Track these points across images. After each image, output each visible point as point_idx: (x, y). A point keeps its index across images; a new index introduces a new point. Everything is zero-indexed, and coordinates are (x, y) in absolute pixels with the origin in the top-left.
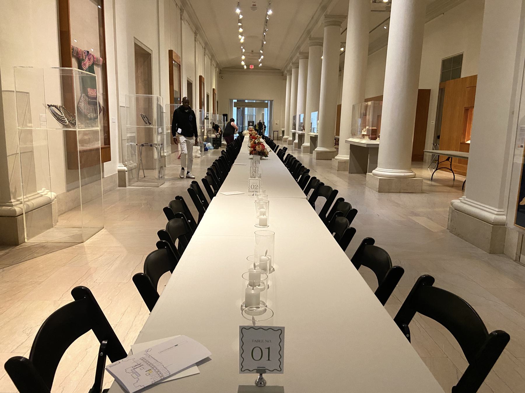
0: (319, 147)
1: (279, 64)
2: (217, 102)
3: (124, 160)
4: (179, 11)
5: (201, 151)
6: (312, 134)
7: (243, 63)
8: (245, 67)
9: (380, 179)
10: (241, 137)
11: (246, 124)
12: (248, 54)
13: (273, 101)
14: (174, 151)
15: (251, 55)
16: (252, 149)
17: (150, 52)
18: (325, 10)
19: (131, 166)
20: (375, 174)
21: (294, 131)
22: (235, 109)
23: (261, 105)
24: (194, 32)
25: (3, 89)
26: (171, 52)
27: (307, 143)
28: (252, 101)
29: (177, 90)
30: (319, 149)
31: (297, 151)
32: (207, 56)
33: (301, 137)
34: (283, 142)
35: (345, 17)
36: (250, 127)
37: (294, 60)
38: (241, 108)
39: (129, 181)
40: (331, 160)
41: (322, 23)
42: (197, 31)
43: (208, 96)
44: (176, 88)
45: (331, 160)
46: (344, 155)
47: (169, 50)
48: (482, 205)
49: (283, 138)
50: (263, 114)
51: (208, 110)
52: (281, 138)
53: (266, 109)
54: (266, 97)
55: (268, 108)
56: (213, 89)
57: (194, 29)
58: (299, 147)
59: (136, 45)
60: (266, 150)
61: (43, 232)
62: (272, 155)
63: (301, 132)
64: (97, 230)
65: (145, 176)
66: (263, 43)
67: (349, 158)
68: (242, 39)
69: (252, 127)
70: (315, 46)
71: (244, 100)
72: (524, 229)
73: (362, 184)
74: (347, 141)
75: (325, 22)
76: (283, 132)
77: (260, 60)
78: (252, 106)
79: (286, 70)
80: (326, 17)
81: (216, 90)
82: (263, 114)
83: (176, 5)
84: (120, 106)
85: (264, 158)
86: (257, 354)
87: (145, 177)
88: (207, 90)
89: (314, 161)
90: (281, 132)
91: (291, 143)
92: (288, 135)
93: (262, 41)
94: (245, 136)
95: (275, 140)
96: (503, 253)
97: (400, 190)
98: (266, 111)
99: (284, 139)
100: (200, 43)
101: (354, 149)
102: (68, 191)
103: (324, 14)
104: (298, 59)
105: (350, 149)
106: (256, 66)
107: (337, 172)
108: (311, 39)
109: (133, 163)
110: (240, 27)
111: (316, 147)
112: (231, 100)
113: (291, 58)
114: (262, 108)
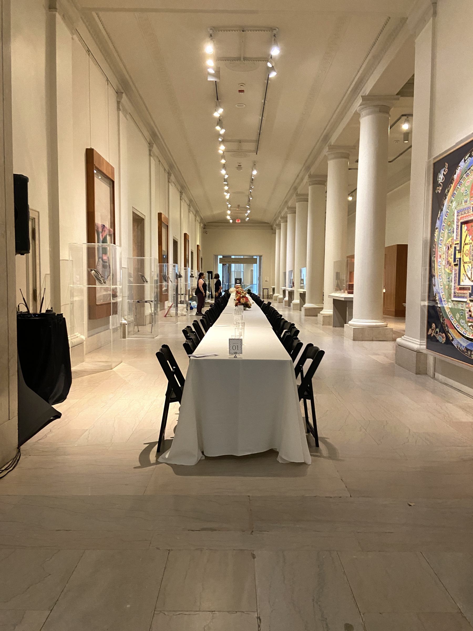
0: (355, 318)
1: (268, 218)
2: (202, 258)
3: (124, 315)
4: (167, 175)
5: (187, 310)
6: (302, 291)
7: (228, 217)
8: (231, 221)
9: (354, 328)
10: (228, 295)
11: (233, 282)
12: (235, 209)
13: (262, 256)
14: (161, 309)
15: (237, 209)
16: (237, 301)
17: (143, 217)
18: (309, 171)
19: (129, 320)
20: (351, 325)
21: (284, 288)
22: (220, 266)
23: (250, 260)
24: (180, 191)
25: (61, 259)
26: (160, 215)
27: (296, 301)
28: (239, 257)
29: (165, 250)
30: (307, 305)
31: (287, 309)
32: (191, 212)
33: (291, 294)
34: (273, 301)
35: (355, 147)
36: (237, 285)
37: (282, 214)
38: (227, 265)
39: (128, 334)
40: (317, 316)
41: (307, 182)
42: (171, 171)
43: (192, 253)
44: (164, 248)
45: (317, 316)
46: (328, 310)
47: (158, 213)
48: (413, 339)
49: (273, 296)
50: (252, 270)
51: (192, 268)
52: (271, 296)
53: (255, 265)
54: (253, 252)
55: (257, 264)
56: (198, 246)
57: (179, 188)
58: (290, 306)
59: (134, 213)
60: (249, 302)
61: (79, 364)
62: (254, 305)
63: (291, 289)
64: (119, 363)
65: (139, 330)
66: (250, 199)
67: (332, 313)
68: (227, 196)
69: (239, 285)
70: (302, 202)
71: (230, 256)
72: (472, 367)
73: (341, 335)
74: (330, 296)
75: (310, 181)
76: (274, 289)
77: (246, 215)
78: (239, 262)
79: (280, 216)
80: (310, 176)
81: (200, 246)
82: (251, 270)
83: (165, 170)
84: (123, 267)
85: (247, 309)
86: (234, 348)
87: (138, 331)
88: (192, 247)
89: (303, 317)
90: (272, 290)
91: (281, 301)
92: (279, 293)
93: (249, 197)
94: (232, 294)
95: (265, 298)
96: (426, 374)
97: (373, 338)
98: (255, 267)
99: (275, 297)
100: (185, 201)
101: (336, 302)
102: (89, 337)
103: (308, 174)
104: (286, 213)
105: (333, 304)
106: (243, 220)
107: (322, 326)
108: (297, 195)
109: (130, 317)
110: (225, 185)
111: (304, 303)
112: (216, 256)
113: (280, 212)
114: (252, 264)
